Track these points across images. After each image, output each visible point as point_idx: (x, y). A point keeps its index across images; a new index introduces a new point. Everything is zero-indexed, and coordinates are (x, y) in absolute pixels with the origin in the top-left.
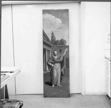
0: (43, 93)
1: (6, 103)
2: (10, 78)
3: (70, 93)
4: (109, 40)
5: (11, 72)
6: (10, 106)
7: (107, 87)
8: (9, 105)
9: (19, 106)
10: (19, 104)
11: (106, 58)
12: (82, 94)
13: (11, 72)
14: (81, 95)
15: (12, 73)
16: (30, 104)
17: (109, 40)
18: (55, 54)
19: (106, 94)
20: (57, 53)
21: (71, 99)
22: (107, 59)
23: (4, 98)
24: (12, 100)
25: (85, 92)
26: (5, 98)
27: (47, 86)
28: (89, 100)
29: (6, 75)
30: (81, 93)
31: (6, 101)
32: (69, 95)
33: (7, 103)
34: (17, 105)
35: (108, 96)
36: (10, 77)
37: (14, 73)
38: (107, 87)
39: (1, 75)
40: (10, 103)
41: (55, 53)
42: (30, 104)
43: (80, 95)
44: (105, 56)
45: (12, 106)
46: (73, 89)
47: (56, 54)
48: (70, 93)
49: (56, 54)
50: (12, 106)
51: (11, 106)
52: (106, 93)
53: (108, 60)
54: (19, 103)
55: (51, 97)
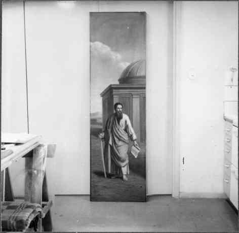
0: (89, 194)
1: (6, 210)
2: (15, 156)
3: (147, 195)
4: (232, 81)
5: (17, 144)
6: (13, 215)
7: (227, 181)
8: (19, 215)
9: (33, 216)
10: (33, 213)
11: (225, 120)
12: (173, 196)
13: (17, 144)
14: (172, 197)
15: (19, 147)
16: (61, 216)
17: (232, 81)
18: (118, 110)
19: (225, 197)
20: (122, 108)
21: (151, 203)
22: (226, 122)
23: (43, 201)
24: (19, 204)
25: (181, 191)
26: (5, 200)
27: (96, 178)
28: (193, 207)
29: (5, 149)
30: (171, 195)
31: (6, 207)
32: (142, 197)
33: (8, 210)
34: (29, 214)
35: (228, 201)
36: (12, 153)
37: (24, 145)
38: (227, 181)
39: (3, 149)
40: (13, 210)
41: (119, 108)
42: (61, 216)
43: (170, 197)
44: (224, 117)
45: (16, 215)
46: (155, 183)
47: (121, 110)
48: (147, 195)
49: (121, 110)
50: (17, 217)
51: (14, 217)
52: (225, 195)
53: (229, 123)
54: (32, 210)
55: (106, 201)
